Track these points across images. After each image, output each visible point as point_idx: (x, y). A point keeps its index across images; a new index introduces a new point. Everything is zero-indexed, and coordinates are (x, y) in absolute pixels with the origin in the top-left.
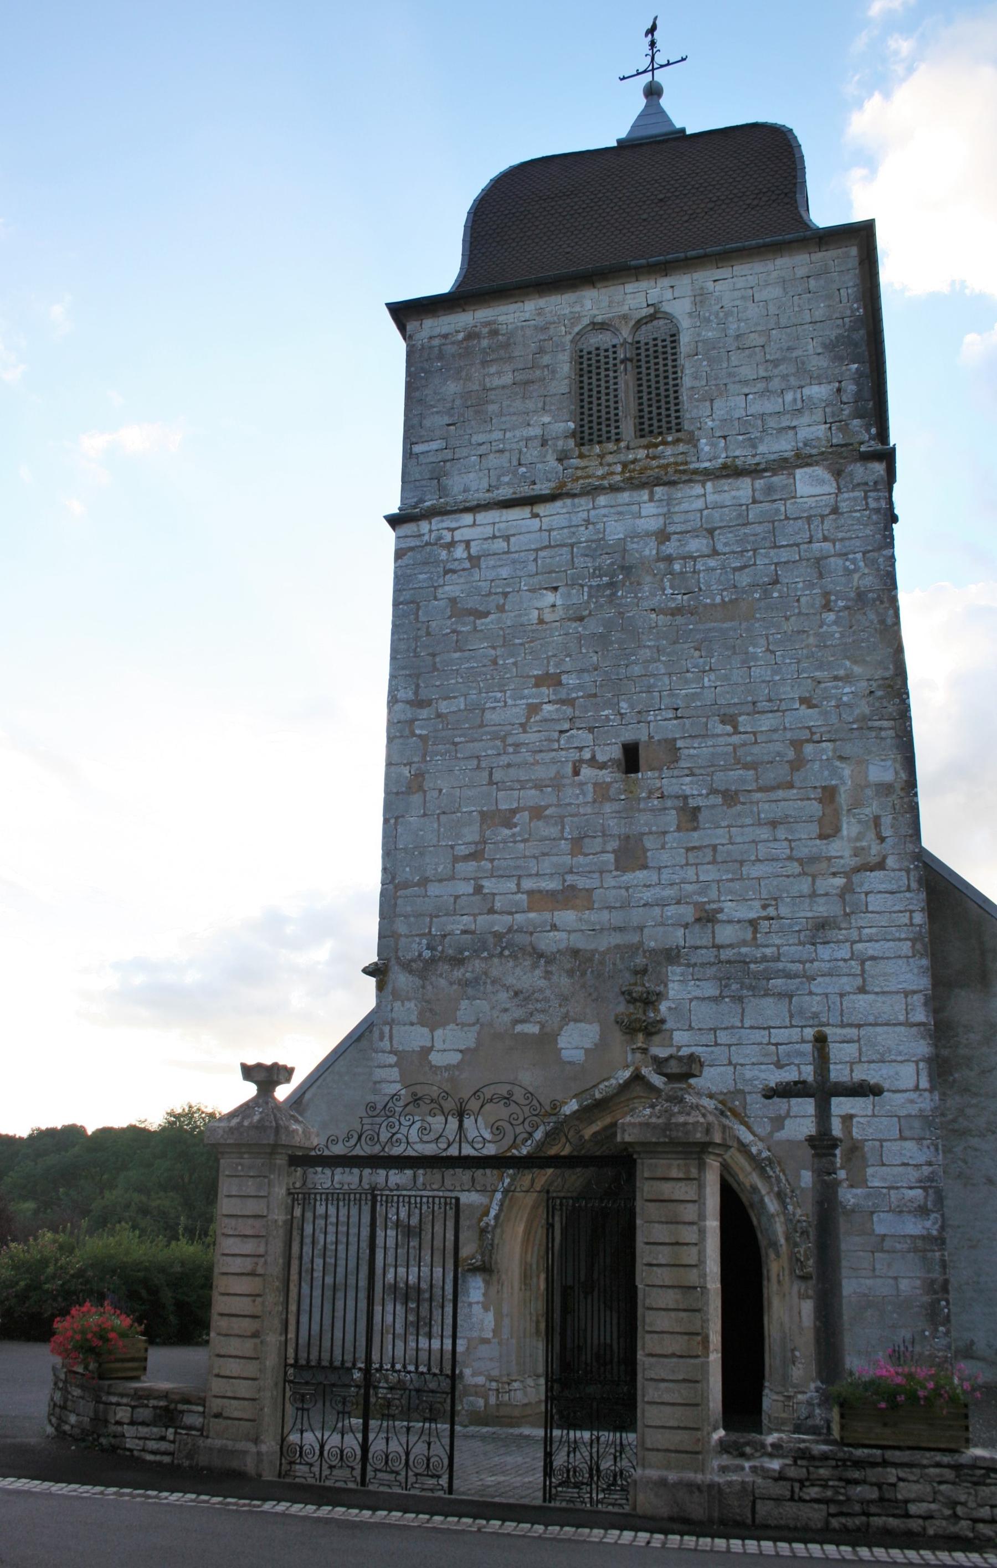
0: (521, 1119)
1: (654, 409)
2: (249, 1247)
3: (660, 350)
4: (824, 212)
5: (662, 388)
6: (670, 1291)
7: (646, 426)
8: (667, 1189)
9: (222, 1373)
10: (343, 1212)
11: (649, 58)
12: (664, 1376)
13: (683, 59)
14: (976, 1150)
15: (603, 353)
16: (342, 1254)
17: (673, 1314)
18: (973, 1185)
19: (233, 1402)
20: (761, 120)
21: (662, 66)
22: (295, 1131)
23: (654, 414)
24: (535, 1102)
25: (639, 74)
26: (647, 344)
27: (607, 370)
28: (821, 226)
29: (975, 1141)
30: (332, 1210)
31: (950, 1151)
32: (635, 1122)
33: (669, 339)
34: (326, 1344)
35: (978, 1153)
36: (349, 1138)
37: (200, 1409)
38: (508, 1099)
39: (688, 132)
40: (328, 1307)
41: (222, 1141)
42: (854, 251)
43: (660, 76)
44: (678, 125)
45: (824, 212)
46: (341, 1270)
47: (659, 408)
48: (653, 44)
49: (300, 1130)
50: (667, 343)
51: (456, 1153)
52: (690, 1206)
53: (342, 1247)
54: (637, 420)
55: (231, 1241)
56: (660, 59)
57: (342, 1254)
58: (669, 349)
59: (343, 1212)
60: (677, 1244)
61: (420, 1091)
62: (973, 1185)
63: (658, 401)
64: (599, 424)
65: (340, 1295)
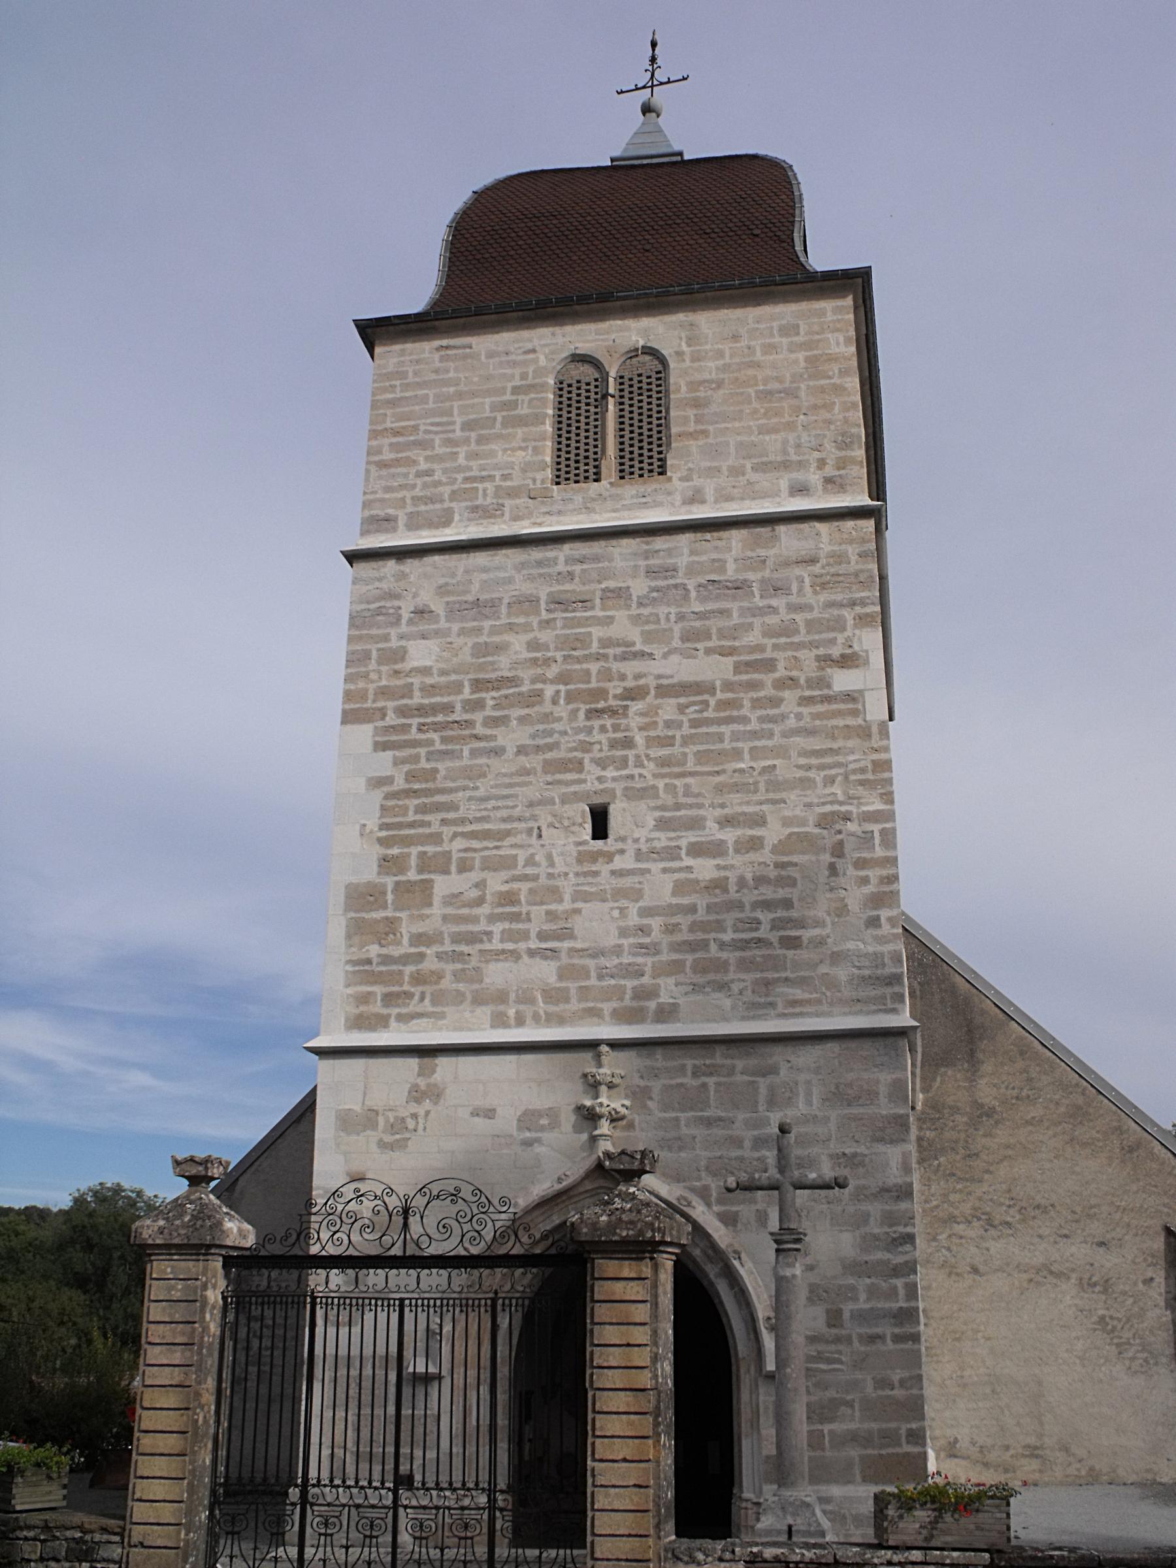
0: (469, 1216)
1: (636, 449)
2: (177, 1357)
3: (645, 387)
4: (822, 256)
5: (646, 427)
6: (622, 1393)
7: (626, 467)
8: (618, 1289)
9: (144, 1498)
10: (280, 1314)
11: (649, 74)
12: (614, 1482)
13: (684, 79)
14: (961, 1237)
15: (584, 387)
16: (278, 1361)
17: (624, 1417)
18: (957, 1274)
19: (156, 1527)
20: (761, 152)
21: (661, 84)
22: (231, 1229)
23: (636, 455)
24: (483, 1199)
25: (637, 89)
26: (631, 379)
27: (588, 404)
28: (819, 270)
29: (960, 1228)
30: (268, 1313)
31: (934, 1239)
32: (592, 1216)
33: (654, 376)
34: (260, 1463)
35: (963, 1241)
36: (287, 1237)
37: (117, 1539)
38: (455, 1196)
39: (686, 157)
40: (262, 1421)
41: (150, 1242)
42: (849, 301)
43: (660, 96)
44: (677, 148)
45: (822, 256)
46: (276, 1379)
47: (641, 448)
48: (653, 60)
49: (235, 1230)
50: (653, 380)
51: (400, 1253)
52: (640, 1305)
53: (278, 1353)
54: (557, 426)
55: (158, 1349)
56: (660, 76)
57: (278, 1361)
58: (653, 387)
59: (280, 1314)
60: (628, 1345)
61: (363, 1187)
62: (957, 1274)
63: (641, 441)
64: (577, 462)
65: (275, 1407)
